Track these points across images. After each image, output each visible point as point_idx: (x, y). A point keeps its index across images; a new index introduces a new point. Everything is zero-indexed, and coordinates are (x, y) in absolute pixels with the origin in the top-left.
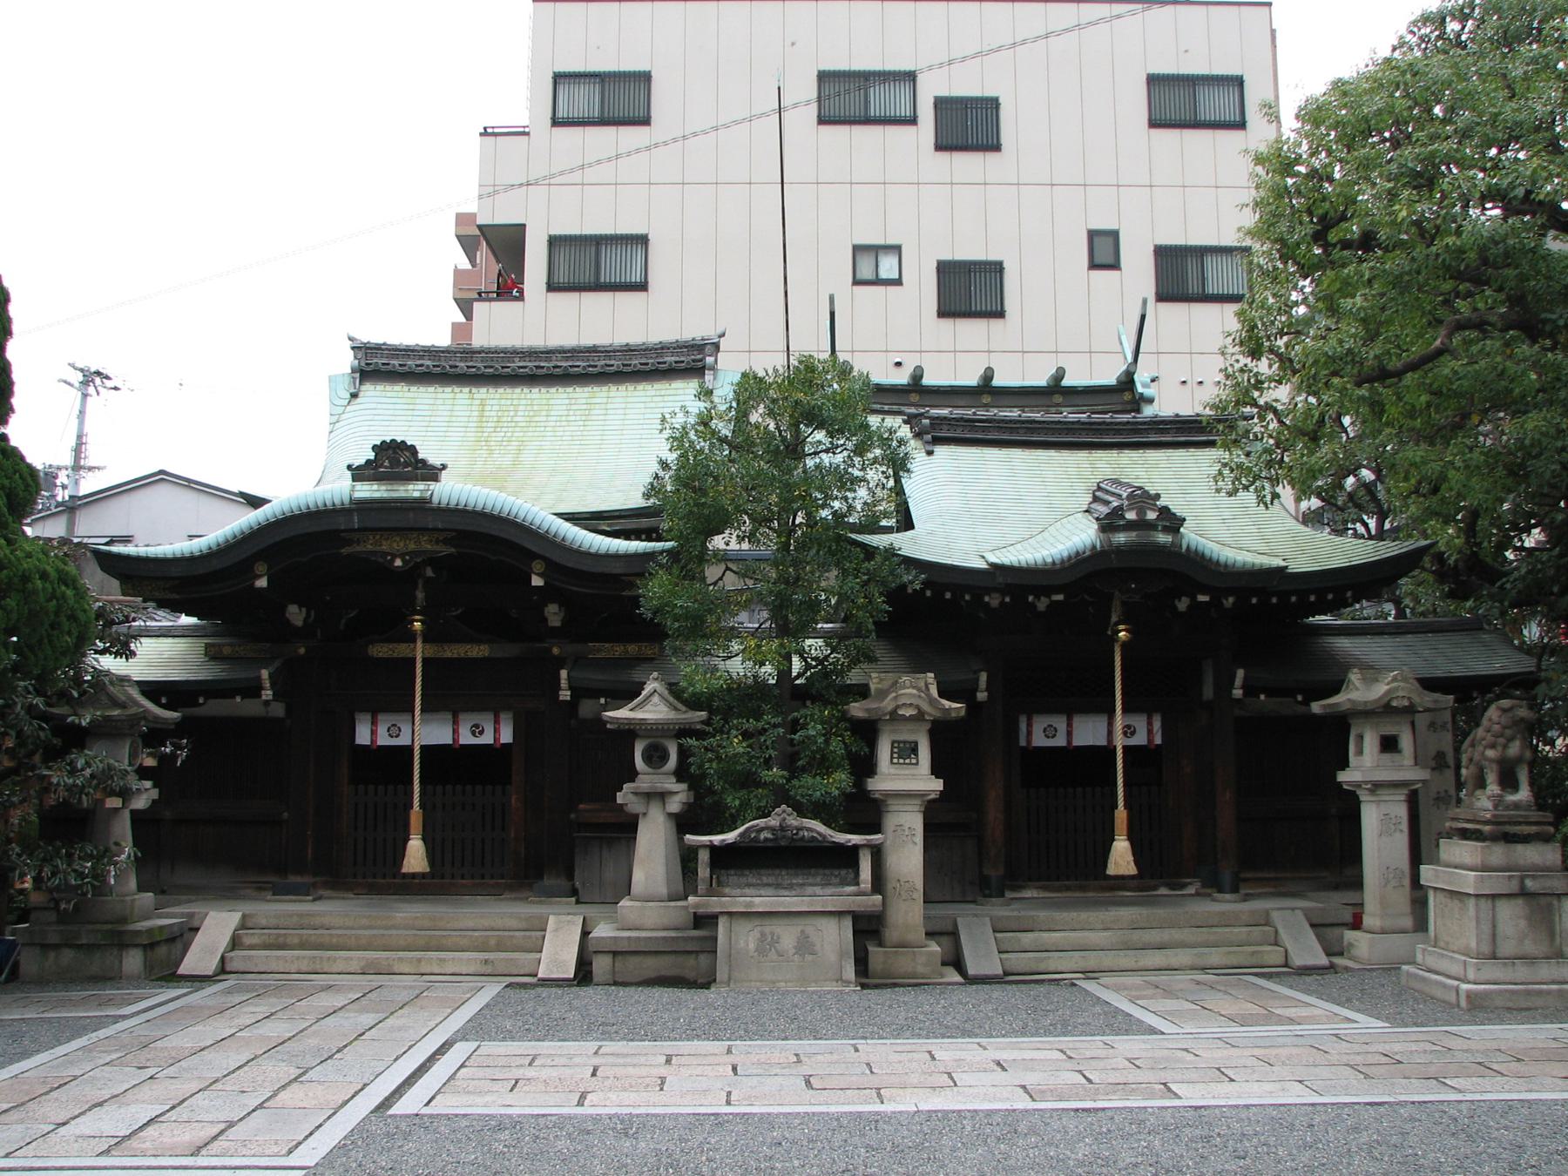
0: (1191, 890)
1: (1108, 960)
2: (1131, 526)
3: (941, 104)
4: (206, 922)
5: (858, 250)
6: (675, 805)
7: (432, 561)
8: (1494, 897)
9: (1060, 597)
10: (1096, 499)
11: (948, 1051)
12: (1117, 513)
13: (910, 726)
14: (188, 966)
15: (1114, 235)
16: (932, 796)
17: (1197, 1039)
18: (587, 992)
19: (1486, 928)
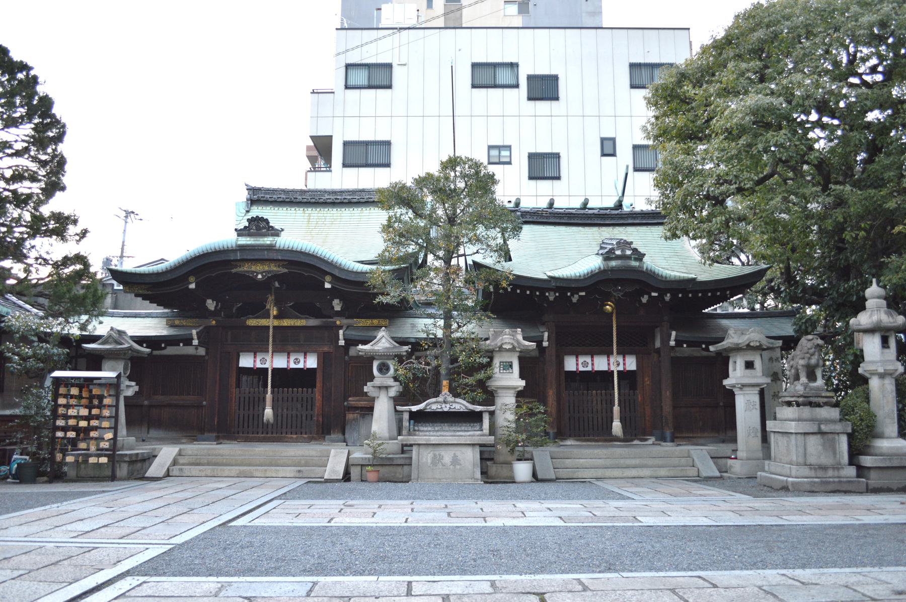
0: (650, 442)
1: (608, 473)
2: (618, 258)
3: (530, 78)
4: (161, 453)
5: (490, 147)
6: (393, 392)
7: (276, 277)
8: (805, 434)
9: (583, 294)
10: (602, 248)
11: (522, 505)
12: (611, 251)
13: (509, 354)
14: (150, 473)
15: (613, 140)
16: (520, 389)
17: (651, 496)
18: (347, 485)
19: (801, 450)
